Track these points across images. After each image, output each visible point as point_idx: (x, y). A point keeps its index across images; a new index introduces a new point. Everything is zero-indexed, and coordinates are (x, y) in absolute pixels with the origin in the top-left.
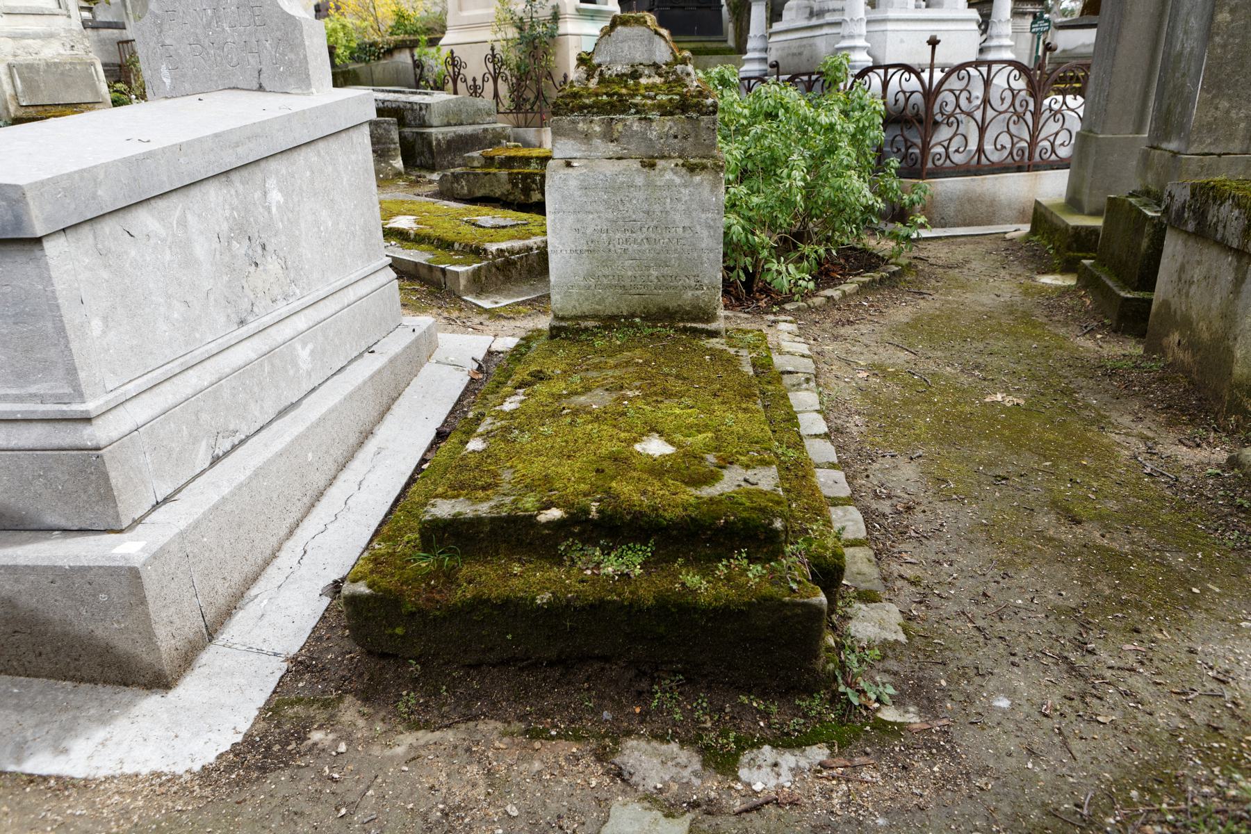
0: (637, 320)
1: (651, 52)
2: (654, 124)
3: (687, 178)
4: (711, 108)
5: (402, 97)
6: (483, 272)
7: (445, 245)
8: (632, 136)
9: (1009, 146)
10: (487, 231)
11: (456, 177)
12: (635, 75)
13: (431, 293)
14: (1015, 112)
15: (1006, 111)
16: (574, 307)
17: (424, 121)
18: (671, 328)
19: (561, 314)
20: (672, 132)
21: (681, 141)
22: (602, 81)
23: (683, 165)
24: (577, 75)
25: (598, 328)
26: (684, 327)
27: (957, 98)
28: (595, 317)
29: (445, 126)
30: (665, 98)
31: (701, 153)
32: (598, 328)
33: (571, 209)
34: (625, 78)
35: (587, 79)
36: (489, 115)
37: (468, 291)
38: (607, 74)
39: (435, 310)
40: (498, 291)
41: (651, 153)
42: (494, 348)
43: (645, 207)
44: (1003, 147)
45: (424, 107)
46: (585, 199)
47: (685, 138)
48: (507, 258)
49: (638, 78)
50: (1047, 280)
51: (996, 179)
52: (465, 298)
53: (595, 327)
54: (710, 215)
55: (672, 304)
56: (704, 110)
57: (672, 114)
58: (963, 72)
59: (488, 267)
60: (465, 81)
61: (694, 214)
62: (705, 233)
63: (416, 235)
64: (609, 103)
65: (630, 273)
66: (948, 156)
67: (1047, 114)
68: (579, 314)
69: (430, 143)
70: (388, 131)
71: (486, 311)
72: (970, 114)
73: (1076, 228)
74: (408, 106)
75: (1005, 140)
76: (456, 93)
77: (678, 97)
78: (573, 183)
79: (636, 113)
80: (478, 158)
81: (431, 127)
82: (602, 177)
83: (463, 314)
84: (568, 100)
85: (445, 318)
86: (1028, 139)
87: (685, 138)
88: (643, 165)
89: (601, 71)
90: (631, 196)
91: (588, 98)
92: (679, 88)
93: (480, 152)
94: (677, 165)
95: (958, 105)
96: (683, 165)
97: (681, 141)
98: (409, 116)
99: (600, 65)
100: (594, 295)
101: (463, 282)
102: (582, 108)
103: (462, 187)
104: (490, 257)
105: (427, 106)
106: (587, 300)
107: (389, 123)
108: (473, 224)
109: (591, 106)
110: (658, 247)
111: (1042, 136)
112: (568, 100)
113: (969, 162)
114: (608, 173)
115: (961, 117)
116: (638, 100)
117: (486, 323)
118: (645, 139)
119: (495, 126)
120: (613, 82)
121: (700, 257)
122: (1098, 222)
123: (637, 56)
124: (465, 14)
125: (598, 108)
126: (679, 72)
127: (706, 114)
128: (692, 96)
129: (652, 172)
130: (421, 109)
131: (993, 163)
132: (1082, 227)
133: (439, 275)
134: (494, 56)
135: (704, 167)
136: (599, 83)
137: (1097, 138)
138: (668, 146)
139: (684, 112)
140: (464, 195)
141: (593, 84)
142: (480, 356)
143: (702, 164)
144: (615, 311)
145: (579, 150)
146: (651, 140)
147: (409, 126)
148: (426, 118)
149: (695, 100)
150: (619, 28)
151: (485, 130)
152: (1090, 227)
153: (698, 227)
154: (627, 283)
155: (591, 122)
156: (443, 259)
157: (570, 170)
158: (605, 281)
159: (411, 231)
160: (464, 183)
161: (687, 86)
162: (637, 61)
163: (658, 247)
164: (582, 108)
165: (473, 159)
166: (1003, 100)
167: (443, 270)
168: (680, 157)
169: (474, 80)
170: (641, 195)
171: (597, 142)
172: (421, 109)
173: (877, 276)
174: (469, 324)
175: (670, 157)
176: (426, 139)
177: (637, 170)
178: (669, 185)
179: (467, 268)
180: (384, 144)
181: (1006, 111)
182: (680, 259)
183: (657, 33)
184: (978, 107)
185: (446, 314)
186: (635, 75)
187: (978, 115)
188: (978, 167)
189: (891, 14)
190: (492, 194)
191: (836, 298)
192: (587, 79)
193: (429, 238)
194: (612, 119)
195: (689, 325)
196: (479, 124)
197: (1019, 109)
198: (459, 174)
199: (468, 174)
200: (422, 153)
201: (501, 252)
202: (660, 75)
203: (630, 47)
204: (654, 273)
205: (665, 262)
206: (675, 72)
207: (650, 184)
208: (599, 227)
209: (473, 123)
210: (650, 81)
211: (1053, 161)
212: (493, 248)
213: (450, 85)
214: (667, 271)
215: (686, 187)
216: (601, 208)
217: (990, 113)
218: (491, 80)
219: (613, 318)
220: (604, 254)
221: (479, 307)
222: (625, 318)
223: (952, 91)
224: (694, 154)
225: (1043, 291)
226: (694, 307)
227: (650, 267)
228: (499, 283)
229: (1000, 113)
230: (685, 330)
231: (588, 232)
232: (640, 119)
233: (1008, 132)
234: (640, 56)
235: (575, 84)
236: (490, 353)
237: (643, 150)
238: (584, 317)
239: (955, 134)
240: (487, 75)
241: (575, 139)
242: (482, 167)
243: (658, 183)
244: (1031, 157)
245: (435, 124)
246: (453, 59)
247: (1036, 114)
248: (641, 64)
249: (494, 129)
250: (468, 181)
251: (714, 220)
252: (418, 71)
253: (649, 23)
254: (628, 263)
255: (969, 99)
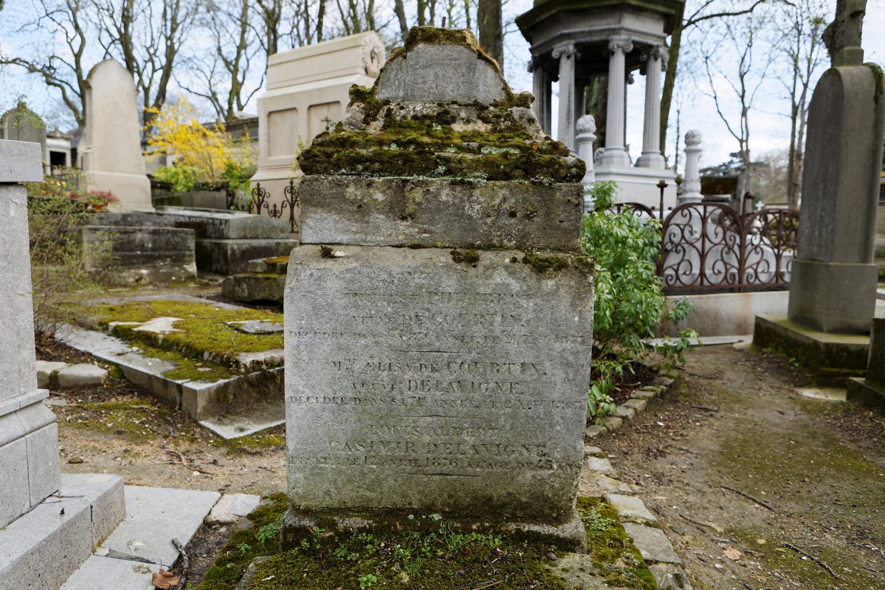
0: (437, 517)
1: (472, 85)
2: (477, 192)
3: (532, 282)
4: (574, 170)
5: (208, 215)
6: (231, 389)
7: (193, 353)
8: (438, 211)
9: (723, 271)
10: (249, 337)
11: (238, 282)
12: (445, 118)
13: (161, 416)
14: (726, 245)
15: (719, 244)
16: (327, 493)
17: (223, 234)
18: (496, 534)
19: (303, 504)
20: (506, 206)
21: (521, 221)
22: (390, 122)
23: (526, 261)
24: (348, 115)
25: (368, 531)
26: (518, 531)
27: (682, 231)
28: (363, 510)
29: (242, 238)
30: (495, 152)
31: (554, 242)
32: (368, 531)
33: (328, 328)
34: (428, 122)
35: (366, 122)
36: (282, 231)
37: (208, 413)
38: (399, 115)
39: (159, 441)
40: (249, 413)
41: (470, 240)
42: (213, 518)
43: (458, 328)
44: (719, 272)
45: (223, 222)
46: (353, 313)
47: (529, 217)
48: (265, 371)
49: (449, 123)
50: (809, 393)
51: (718, 297)
52: (202, 423)
53: (361, 530)
54: (568, 345)
55: (498, 492)
56: (563, 172)
57: (507, 177)
58: (686, 211)
59: (238, 384)
60: (267, 207)
61: (542, 342)
62: (559, 375)
63: (165, 340)
64: (400, 155)
65: (426, 439)
66: (678, 278)
67: (750, 247)
68: (336, 505)
69: (225, 252)
70: (184, 240)
71: (225, 442)
72: (692, 245)
73: (827, 345)
74: (210, 221)
75: (720, 266)
76: (259, 213)
77: (517, 152)
78: (333, 285)
79: (446, 173)
80: (261, 264)
81: (228, 238)
82: (383, 276)
83: (195, 447)
84: (331, 149)
85: (168, 453)
86: (737, 265)
87: (529, 217)
88: (457, 258)
89: (389, 110)
90: (434, 309)
91: (364, 147)
92: (517, 139)
93: (265, 259)
94: (514, 260)
95: (683, 237)
96: (526, 261)
97: (521, 221)
98: (210, 230)
99: (387, 102)
100: (363, 474)
101: (201, 403)
102: (353, 162)
103: (243, 290)
104: (243, 370)
105: (227, 221)
106: (350, 481)
107: (186, 233)
108: (237, 329)
109: (370, 160)
110: (477, 396)
111: (747, 265)
112: (331, 149)
113: (693, 284)
114: (395, 270)
115: (686, 246)
116: (450, 152)
117: (222, 461)
118: (461, 216)
119: (287, 241)
120: (409, 127)
121: (548, 414)
122: (865, 341)
123: (449, 89)
124: (273, 158)
125: (382, 162)
126: (516, 116)
127: (564, 179)
128: (540, 150)
129: (472, 271)
130: (221, 224)
131: (685, 285)
132: (833, 345)
133: (174, 392)
134: (292, 188)
135: (561, 266)
136: (385, 128)
137: (828, 266)
138: (500, 228)
139: (527, 174)
140: (245, 298)
141: (375, 128)
142: (186, 533)
143: (558, 260)
144: (398, 501)
145: (345, 231)
146: (470, 218)
147: (210, 237)
148: (225, 231)
149: (547, 157)
150: (421, 46)
151: (278, 244)
152: (841, 344)
153: (548, 364)
154: (422, 455)
155: (369, 185)
156: (184, 372)
157: (329, 263)
158: (383, 451)
159: (161, 336)
160: (245, 287)
161: (529, 137)
162: (448, 98)
163: (477, 396)
164: (353, 162)
165: (256, 265)
166: (716, 234)
167: (180, 387)
168: (518, 248)
169: (275, 206)
170: (451, 308)
171: (379, 218)
172: (221, 224)
173: (659, 389)
174: (197, 463)
175: (502, 248)
176: (222, 249)
177: (446, 266)
178: (501, 293)
179: (210, 385)
180: (180, 250)
181: (719, 244)
182: (514, 416)
183: (480, 56)
184: (698, 240)
185: (171, 447)
186: (445, 118)
187: (699, 245)
188: (701, 288)
189: (613, 169)
190: (271, 297)
191: (630, 417)
192: (366, 122)
193: (178, 344)
194: (406, 181)
195: (526, 528)
196: (272, 238)
197: (730, 243)
198: (241, 278)
199: (249, 278)
200: (218, 261)
201: (257, 364)
202: (485, 120)
203: (437, 76)
204: (469, 439)
205: (489, 421)
206: (509, 116)
207: (467, 291)
208: (376, 361)
209: (268, 238)
210: (470, 128)
211: (677, 287)
212: (247, 359)
213: (255, 209)
214: (490, 436)
215: (528, 296)
216: (381, 328)
217: (708, 245)
218: (288, 207)
219: (394, 512)
220: (382, 405)
221: (218, 436)
222: (416, 513)
223: (678, 225)
224: (543, 243)
225: (807, 406)
226: (535, 497)
227: (462, 429)
228: (252, 401)
229: (715, 245)
230: (520, 536)
231: (356, 367)
232: (453, 183)
233: (722, 260)
234: (452, 90)
235: (346, 128)
236: (207, 525)
237: (456, 234)
238: (345, 511)
239: (682, 260)
240: (286, 203)
241: (340, 212)
242: (264, 272)
243: (482, 290)
244: (740, 281)
245: (232, 236)
246: (259, 189)
247: (742, 247)
248: (454, 103)
249: (286, 243)
250: (249, 285)
251: (576, 353)
252: (230, 198)
253: (469, 41)
254: (423, 422)
255: (691, 233)
